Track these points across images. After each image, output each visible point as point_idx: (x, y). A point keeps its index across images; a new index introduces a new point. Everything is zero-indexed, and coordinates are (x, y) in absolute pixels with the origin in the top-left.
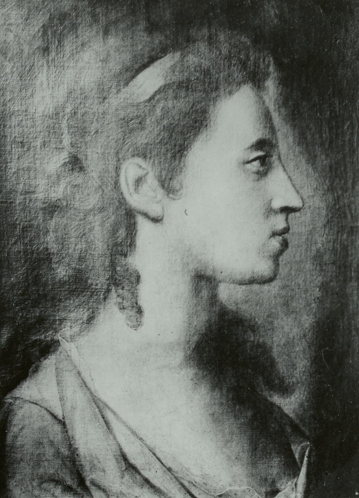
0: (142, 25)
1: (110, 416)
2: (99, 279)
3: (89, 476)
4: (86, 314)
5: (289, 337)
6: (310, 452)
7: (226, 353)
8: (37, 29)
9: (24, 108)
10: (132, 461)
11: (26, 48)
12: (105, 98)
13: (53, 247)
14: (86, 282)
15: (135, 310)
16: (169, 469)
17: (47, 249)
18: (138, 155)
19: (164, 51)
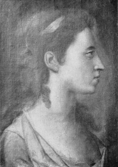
0: (53, 7)
1: (39, 137)
2: (36, 90)
3: (32, 158)
4: (32, 103)
5: (100, 117)
6: (106, 151)
7: (79, 114)
8: (18, 8)
9: (13, 34)
10: (47, 152)
11: (14, 14)
12: (40, 31)
13: (22, 80)
14: (32, 92)
15: (48, 102)
16: (59, 156)
17: (20, 81)
18: (50, 51)
19: (60, 16)
